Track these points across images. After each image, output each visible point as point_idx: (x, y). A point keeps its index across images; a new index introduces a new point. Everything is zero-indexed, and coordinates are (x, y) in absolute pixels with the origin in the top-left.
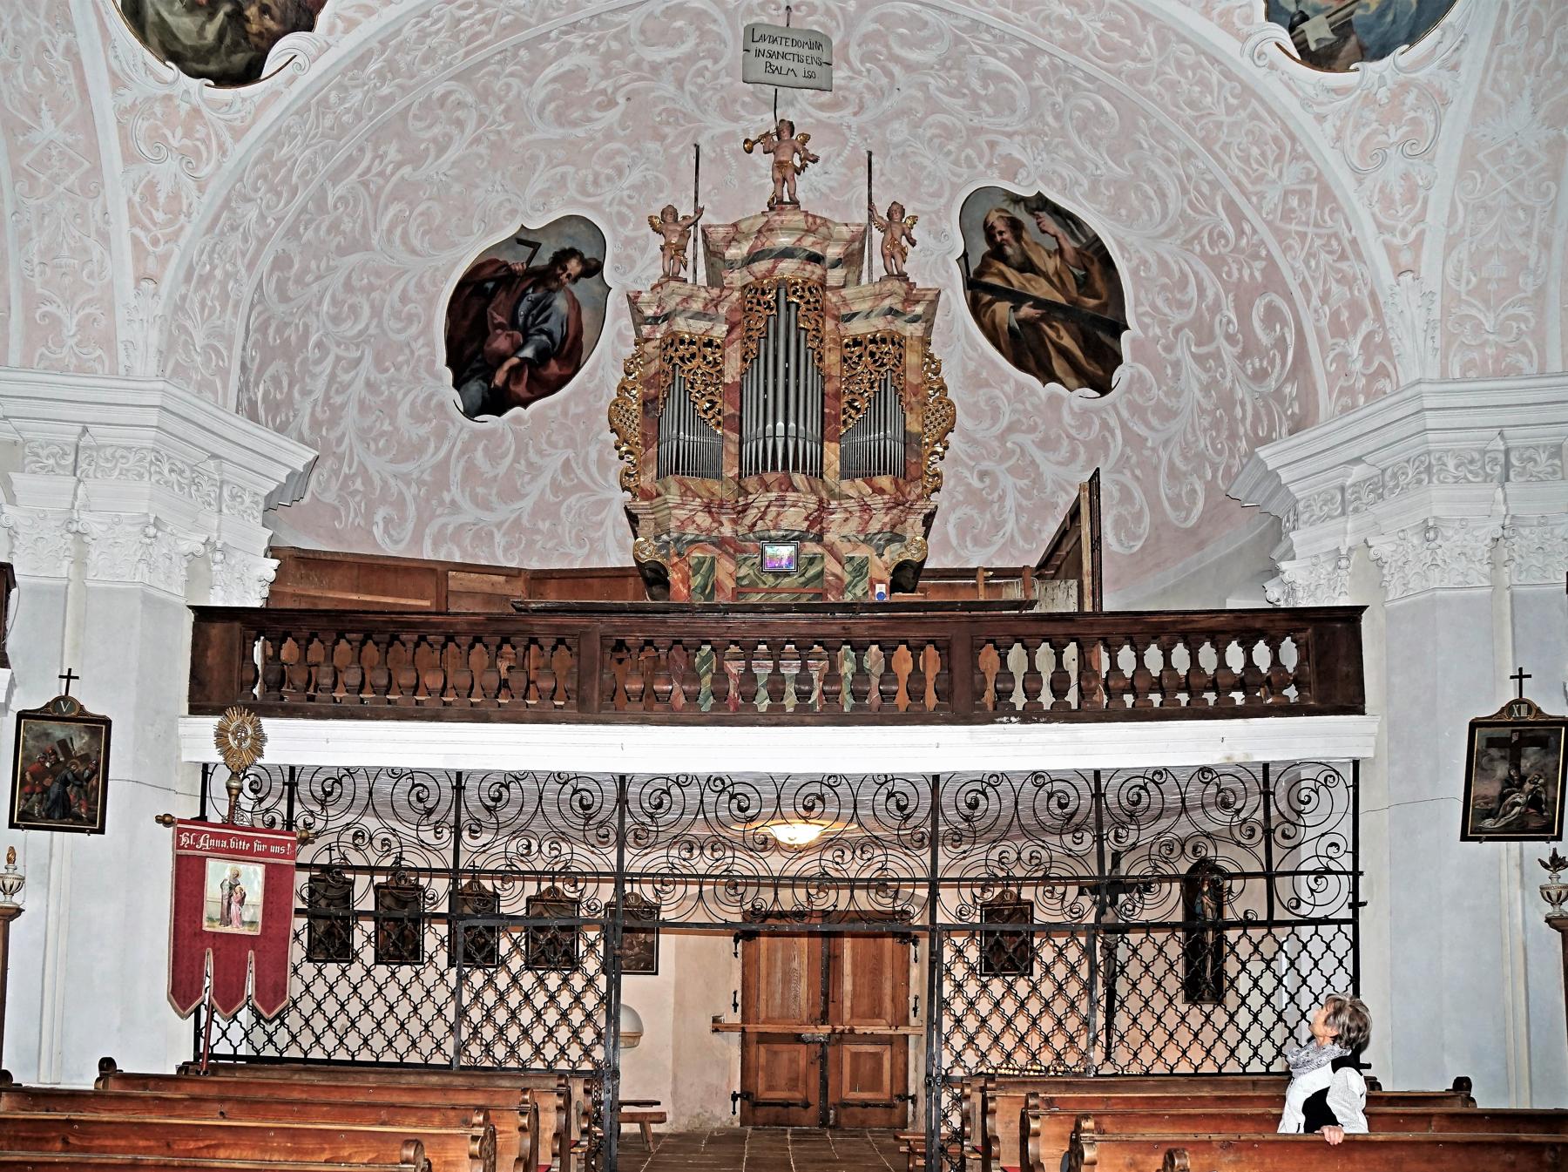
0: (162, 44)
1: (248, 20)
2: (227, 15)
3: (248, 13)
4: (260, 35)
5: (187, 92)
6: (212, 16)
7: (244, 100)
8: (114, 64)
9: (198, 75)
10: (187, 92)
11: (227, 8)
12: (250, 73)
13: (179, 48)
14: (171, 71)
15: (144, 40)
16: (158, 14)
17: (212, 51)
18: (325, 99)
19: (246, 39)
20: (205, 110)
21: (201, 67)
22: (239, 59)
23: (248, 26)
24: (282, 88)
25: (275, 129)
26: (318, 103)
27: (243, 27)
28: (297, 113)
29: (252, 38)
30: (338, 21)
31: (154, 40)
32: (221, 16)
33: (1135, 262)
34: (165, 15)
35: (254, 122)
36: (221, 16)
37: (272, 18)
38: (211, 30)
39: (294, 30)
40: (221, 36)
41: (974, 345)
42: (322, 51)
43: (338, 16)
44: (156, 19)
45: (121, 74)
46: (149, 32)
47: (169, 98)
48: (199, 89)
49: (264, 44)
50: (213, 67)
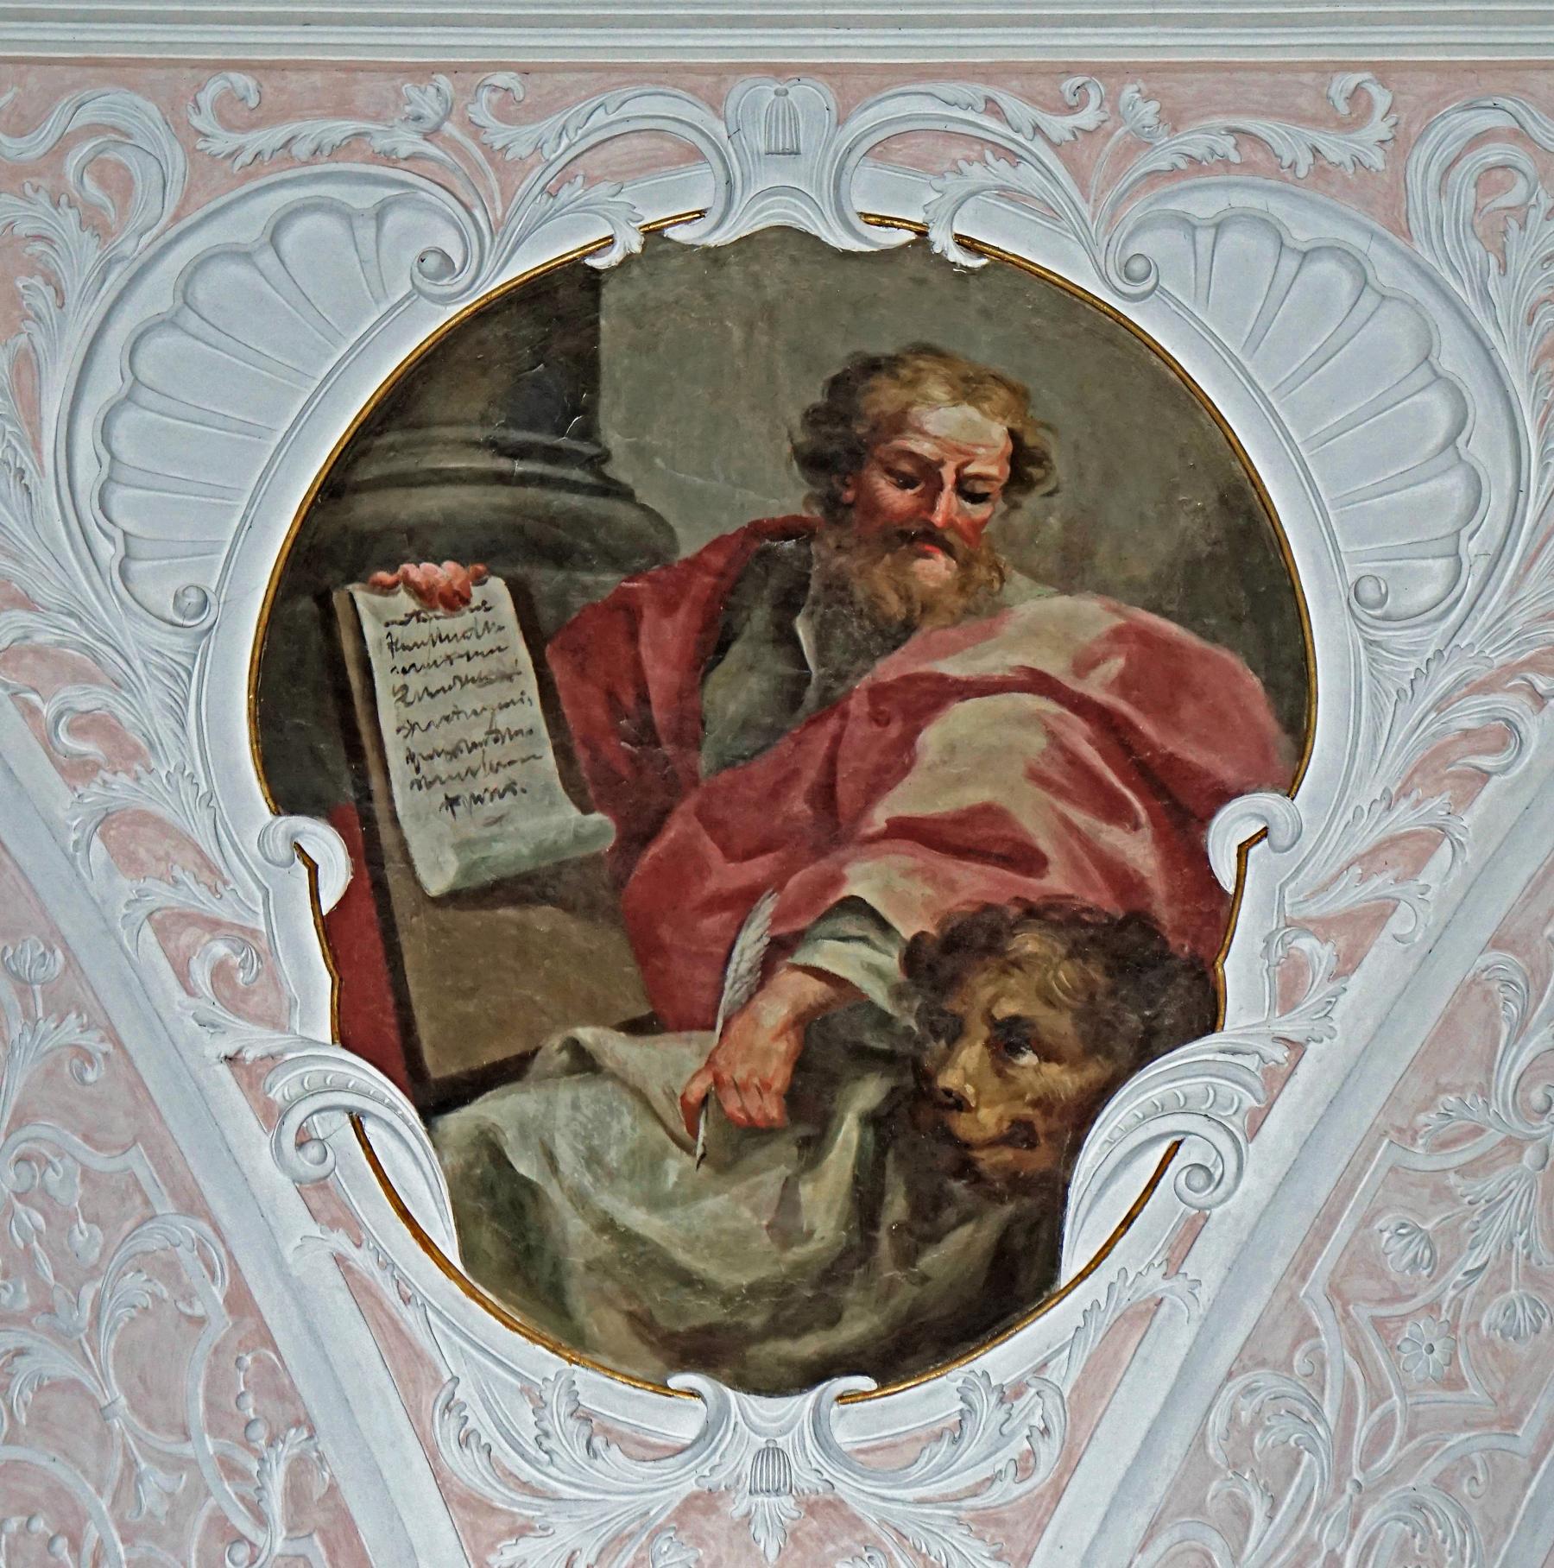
0: (641, 1323)
1: (960, 1105)
2: (872, 1120)
3: (950, 1079)
4: (1020, 1134)
5: (771, 1453)
6: (814, 1147)
7: (1008, 1395)
8: (466, 1467)
9: (813, 1374)
10: (771, 1453)
11: (869, 1093)
12: (1017, 1279)
13: (708, 1312)
14: (689, 1406)
15: (571, 1340)
16: (607, 1225)
17: (836, 1272)
18: (1362, 1259)
19: (965, 1168)
20: (849, 1489)
21: (810, 1346)
22: (958, 1250)
23: (962, 1125)
24: (1155, 1281)
25: (1175, 1448)
26: (1335, 1291)
27: (949, 1136)
28: (1250, 1357)
29: (986, 1159)
30: (1306, 944)
31: (606, 1323)
32: (848, 1133)
33: (1471, 1321)
34: (638, 1219)
35: (1070, 1462)
36: (848, 1133)
37: (1048, 1054)
38: (824, 1200)
39: (1146, 1050)
40: (865, 1202)
41: (1204, 338)
42: (1276, 1080)
43: (1303, 926)
44: (604, 1246)
45: (499, 1495)
46: (578, 1302)
47: (704, 1502)
48: (864, 1414)
49: (1039, 1160)
50: (857, 1327)
